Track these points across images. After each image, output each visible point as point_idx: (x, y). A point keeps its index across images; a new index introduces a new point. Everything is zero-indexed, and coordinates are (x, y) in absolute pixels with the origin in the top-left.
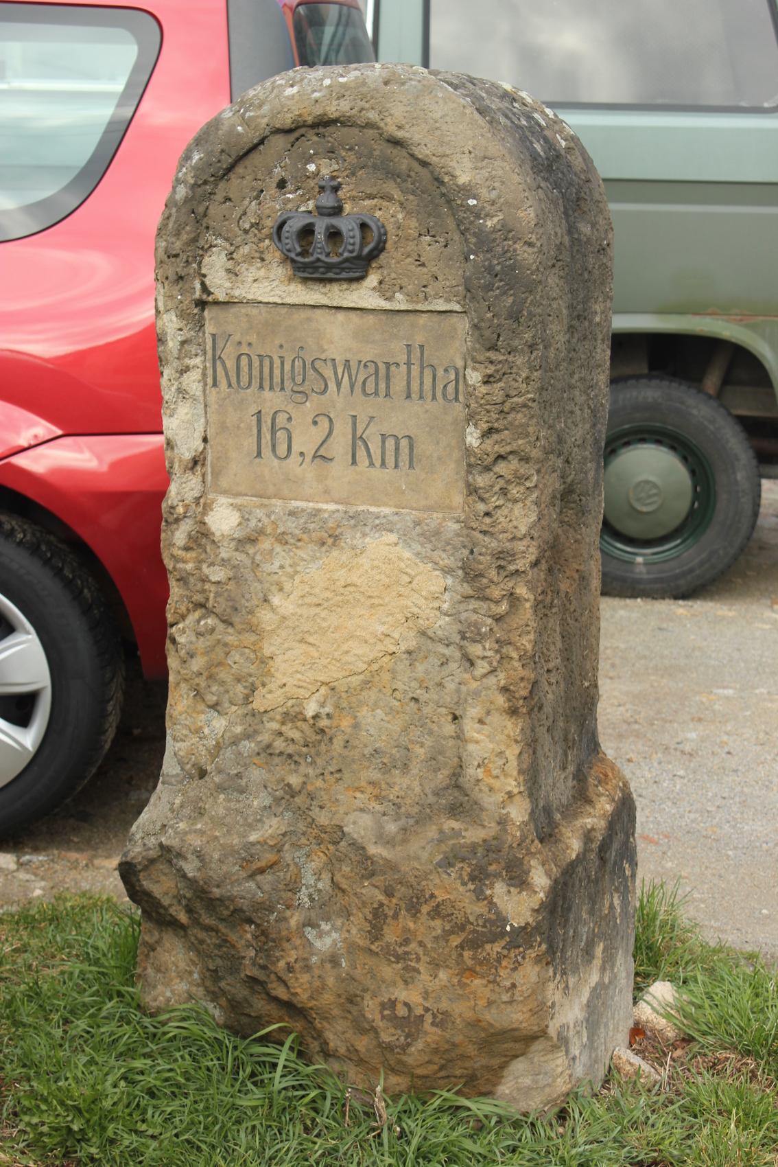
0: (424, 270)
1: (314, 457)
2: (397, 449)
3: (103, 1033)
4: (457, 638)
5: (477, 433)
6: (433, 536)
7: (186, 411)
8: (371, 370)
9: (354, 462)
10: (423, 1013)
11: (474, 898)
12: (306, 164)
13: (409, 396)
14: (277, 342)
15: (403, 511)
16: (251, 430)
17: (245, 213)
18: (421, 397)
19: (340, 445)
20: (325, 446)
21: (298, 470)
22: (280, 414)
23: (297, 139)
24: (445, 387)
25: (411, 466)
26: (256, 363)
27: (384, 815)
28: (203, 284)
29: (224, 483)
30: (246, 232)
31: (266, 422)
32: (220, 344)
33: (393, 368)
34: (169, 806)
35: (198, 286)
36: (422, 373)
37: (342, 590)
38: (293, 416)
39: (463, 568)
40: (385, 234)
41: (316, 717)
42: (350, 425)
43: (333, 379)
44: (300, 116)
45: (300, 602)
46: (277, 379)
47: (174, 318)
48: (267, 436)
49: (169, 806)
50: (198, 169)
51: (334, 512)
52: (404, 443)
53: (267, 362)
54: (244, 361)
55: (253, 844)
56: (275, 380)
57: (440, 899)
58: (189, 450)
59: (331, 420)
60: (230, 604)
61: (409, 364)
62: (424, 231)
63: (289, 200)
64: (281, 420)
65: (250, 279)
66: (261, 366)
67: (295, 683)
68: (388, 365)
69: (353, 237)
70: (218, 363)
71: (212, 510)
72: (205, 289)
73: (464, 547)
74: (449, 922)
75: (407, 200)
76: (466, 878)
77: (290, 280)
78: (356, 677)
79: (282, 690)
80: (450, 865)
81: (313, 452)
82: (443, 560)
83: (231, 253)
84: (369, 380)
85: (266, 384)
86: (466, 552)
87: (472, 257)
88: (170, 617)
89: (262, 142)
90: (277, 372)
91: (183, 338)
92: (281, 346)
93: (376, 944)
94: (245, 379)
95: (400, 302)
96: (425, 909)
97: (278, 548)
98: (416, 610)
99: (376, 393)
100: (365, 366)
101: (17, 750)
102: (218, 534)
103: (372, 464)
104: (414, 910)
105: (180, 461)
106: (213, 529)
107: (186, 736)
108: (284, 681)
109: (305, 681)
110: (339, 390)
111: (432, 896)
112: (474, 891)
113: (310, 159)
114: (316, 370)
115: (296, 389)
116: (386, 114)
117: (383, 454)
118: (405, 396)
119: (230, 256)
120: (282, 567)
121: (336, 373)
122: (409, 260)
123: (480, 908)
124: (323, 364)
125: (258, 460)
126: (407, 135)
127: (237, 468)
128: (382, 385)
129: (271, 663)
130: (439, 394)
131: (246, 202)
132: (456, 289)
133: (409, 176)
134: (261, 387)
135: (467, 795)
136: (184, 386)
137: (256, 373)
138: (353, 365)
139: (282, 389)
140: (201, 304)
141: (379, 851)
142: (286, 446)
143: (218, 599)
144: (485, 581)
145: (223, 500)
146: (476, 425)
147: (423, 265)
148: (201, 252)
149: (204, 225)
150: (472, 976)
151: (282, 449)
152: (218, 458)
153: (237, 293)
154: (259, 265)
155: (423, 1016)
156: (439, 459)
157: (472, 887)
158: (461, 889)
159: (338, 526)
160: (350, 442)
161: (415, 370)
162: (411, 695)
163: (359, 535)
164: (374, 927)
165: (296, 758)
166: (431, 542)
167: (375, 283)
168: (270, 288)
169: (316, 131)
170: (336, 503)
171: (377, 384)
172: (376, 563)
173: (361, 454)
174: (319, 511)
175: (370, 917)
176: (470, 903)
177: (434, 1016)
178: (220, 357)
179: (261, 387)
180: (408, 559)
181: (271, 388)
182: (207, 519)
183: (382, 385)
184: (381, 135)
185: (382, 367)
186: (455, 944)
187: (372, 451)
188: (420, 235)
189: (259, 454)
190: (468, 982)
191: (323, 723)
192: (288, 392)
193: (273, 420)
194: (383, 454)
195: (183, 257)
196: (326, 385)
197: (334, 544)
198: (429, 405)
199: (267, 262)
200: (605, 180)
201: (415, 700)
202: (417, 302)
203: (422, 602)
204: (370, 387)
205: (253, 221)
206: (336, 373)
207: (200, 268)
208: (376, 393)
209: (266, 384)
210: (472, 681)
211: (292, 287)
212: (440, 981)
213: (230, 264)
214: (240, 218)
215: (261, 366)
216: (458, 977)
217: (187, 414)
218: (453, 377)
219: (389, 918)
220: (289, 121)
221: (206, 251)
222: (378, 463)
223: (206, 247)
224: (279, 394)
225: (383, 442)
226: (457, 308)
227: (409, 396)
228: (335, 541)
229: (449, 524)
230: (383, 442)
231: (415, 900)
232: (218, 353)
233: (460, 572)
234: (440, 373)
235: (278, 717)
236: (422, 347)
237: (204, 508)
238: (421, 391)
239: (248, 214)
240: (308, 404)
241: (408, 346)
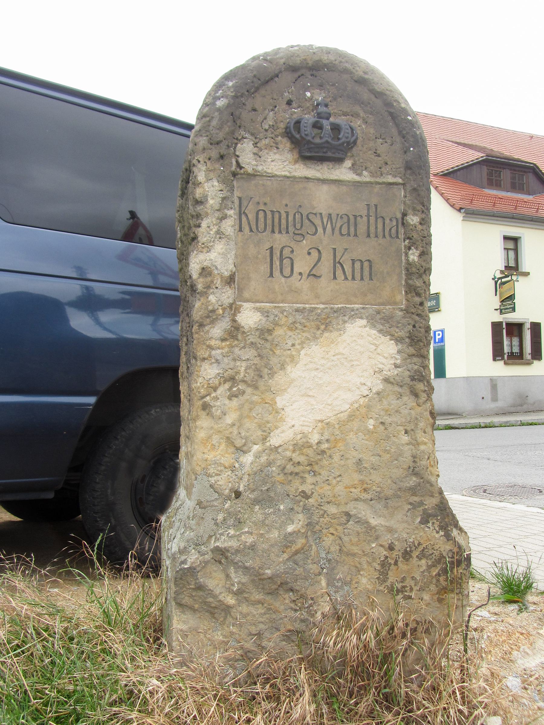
0: (380, 158)
2: (362, 268)
3: (168, 697)
4: (408, 380)
5: (417, 253)
6: (387, 319)
7: (221, 247)
8: (345, 219)
9: (335, 278)
10: (416, 626)
11: (445, 540)
12: (305, 91)
13: (369, 236)
14: (284, 202)
15: (367, 306)
16: (266, 259)
17: (265, 119)
18: (376, 236)
19: (325, 267)
20: (316, 268)
21: (298, 284)
22: (286, 248)
23: (299, 77)
24: (390, 230)
25: (371, 279)
26: (269, 216)
27: (371, 500)
28: (238, 163)
29: (246, 295)
30: (266, 130)
31: (276, 254)
32: (245, 203)
33: (359, 218)
34: (213, 522)
35: (234, 163)
36: (376, 221)
37: (333, 358)
38: (294, 249)
39: (409, 337)
41: (319, 443)
42: (332, 254)
43: (321, 226)
44: (305, 60)
45: (304, 369)
46: (284, 226)
47: (216, 183)
48: (277, 263)
49: (213, 522)
50: (237, 87)
51: (324, 309)
52: (366, 264)
53: (277, 216)
54: (261, 214)
55: (290, 534)
56: (282, 227)
57: (424, 545)
58: (227, 270)
59: (319, 251)
60: (257, 373)
61: (368, 216)
62: (378, 136)
63: (295, 113)
64: (287, 252)
65: (269, 160)
66: (273, 218)
67: (301, 423)
68: (355, 217)
70: (243, 217)
71: (239, 312)
73: (409, 324)
74: (431, 559)
75: (368, 117)
76: (437, 529)
77: (296, 162)
78: (343, 414)
79: (292, 429)
81: (308, 271)
82: (397, 333)
83: (256, 144)
84: (344, 226)
85: (276, 230)
86: (410, 327)
87: (412, 149)
89: (272, 79)
90: (284, 222)
91: (224, 196)
92: (286, 205)
93: (383, 586)
94: (261, 226)
95: (366, 177)
96: (415, 554)
97: (290, 333)
98: (381, 366)
99: (349, 235)
100: (341, 217)
101: (20, 521)
102: (246, 327)
103: (346, 278)
105: (222, 277)
106: (243, 324)
107: (221, 471)
108: (293, 423)
109: (307, 422)
110: (324, 232)
111: (419, 544)
112: (444, 536)
113: (307, 89)
115: (296, 232)
116: (356, 65)
117: (353, 271)
118: (366, 235)
119: (255, 145)
120: (293, 345)
122: (370, 152)
123: (448, 547)
124: (314, 216)
125: (270, 279)
126: (371, 78)
128: (352, 229)
129: (283, 412)
131: (267, 112)
132: (399, 169)
133: (369, 103)
134: (273, 231)
135: (422, 478)
136: (222, 229)
137: (269, 222)
138: (334, 217)
140: (234, 174)
141: (379, 522)
142: (289, 269)
143: (248, 371)
145: (246, 305)
146: (417, 248)
147: (379, 156)
148: (236, 141)
149: (238, 124)
150: (445, 593)
151: (287, 272)
152: (243, 279)
153: (260, 168)
154: (275, 151)
155: (416, 628)
156: (388, 273)
157: (443, 533)
158: (437, 536)
159: (328, 317)
160: (332, 265)
161: (372, 220)
162: (381, 420)
163: (341, 322)
164: (382, 573)
165: (302, 475)
166: (389, 322)
167: (350, 165)
168: (282, 166)
169: (311, 72)
170: (323, 304)
171: (349, 228)
172: (354, 338)
173: (339, 272)
174: (315, 308)
175: (378, 567)
176: (444, 544)
178: (244, 213)
179: (273, 231)
180: (374, 334)
181: (280, 232)
182: (237, 318)
183: (352, 229)
184: (352, 78)
186: (434, 573)
187: (346, 270)
188: (376, 138)
189: (271, 275)
190: (444, 597)
192: (291, 234)
193: (281, 252)
194: (353, 271)
195: (225, 143)
196: (316, 230)
197: (325, 329)
198: (381, 240)
199: (281, 149)
201: (382, 423)
202: (376, 177)
203: (384, 361)
205: (271, 124)
207: (235, 151)
208: (349, 235)
209: (276, 230)
210: (417, 407)
211: (297, 166)
212: (426, 601)
213: (255, 150)
214: (263, 121)
215: (273, 218)
216: (437, 596)
217: (222, 249)
218: (394, 223)
219: (392, 566)
220: (299, 62)
221: (240, 140)
222: (350, 278)
223: (240, 138)
224: (285, 235)
225: (353, 264)
226: (400, 181)
227: (369, 236)
228: (326, 326)
229: (397, 312)
230: (353, 264)
231: (408, 549)
232: (243, 209)
233: (407, 340)
234: (387, 221)
235: (291, 448)
236: (376, 206)
237: (235, 311)
238: (376, 232)
239: (268, 119)
240: (304, 241)
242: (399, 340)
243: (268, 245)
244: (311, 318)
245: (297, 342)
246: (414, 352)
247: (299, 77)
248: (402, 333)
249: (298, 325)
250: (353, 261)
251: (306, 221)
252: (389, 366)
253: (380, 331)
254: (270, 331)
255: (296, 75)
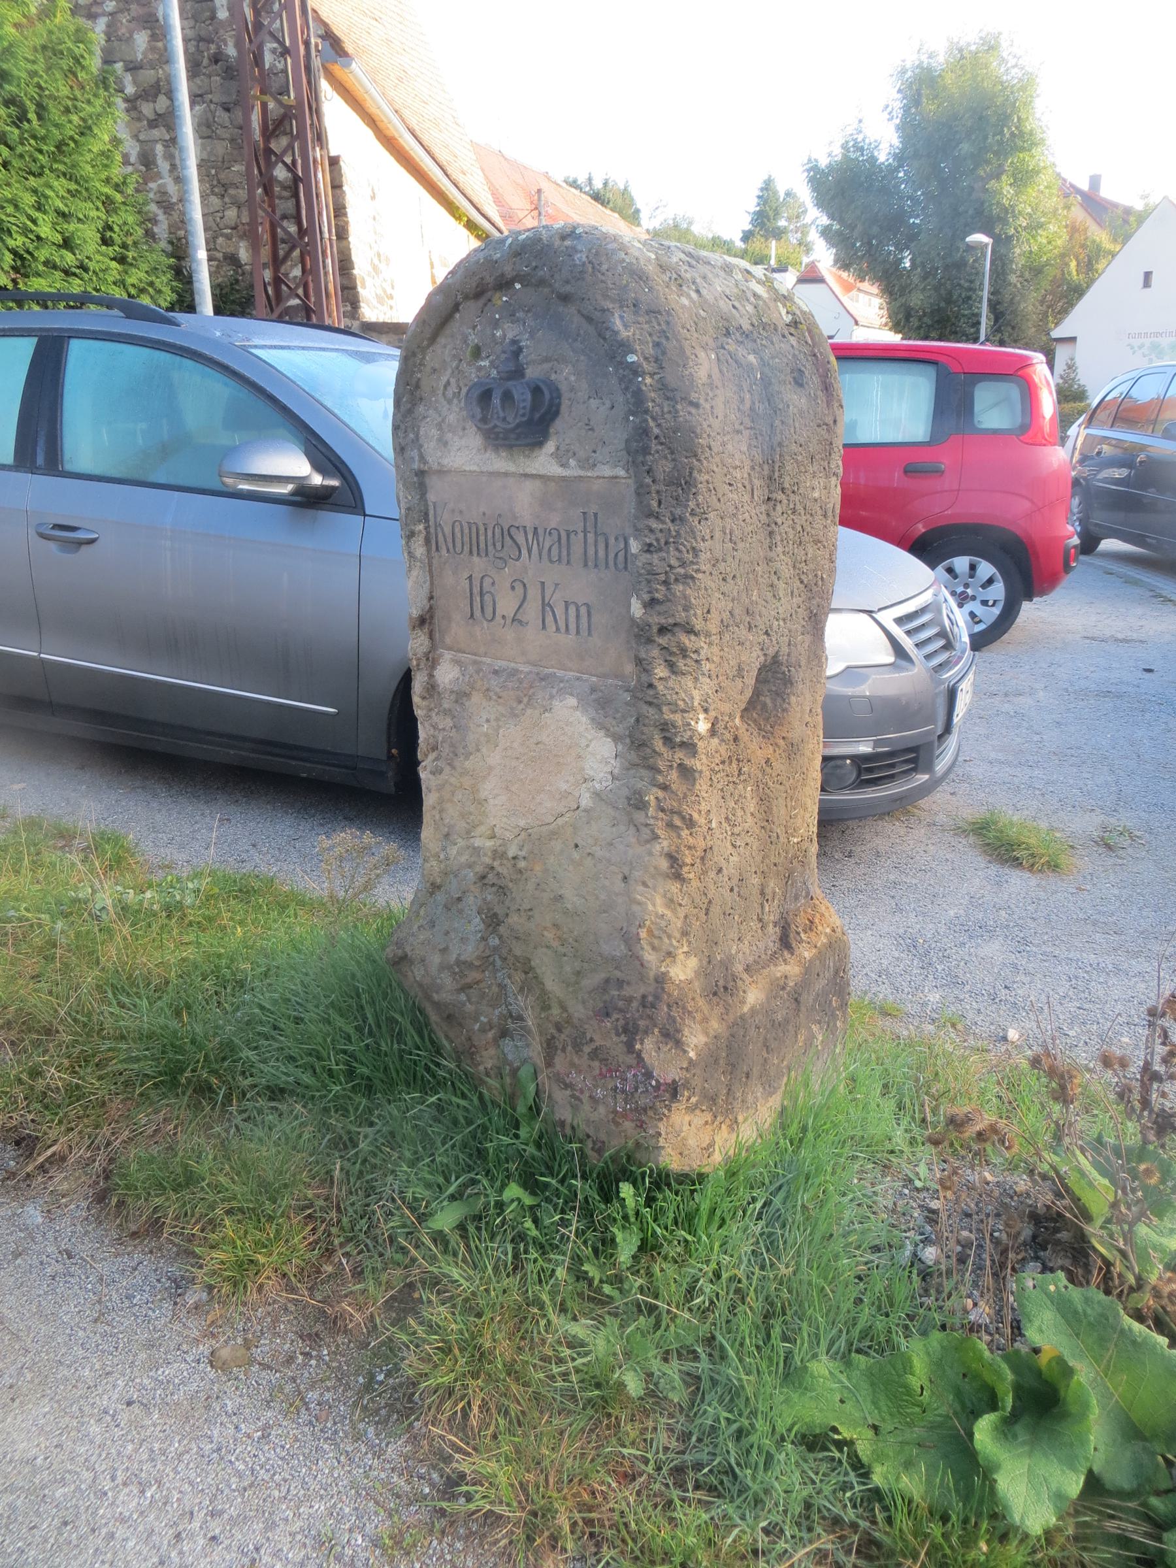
1: (513, 620)
2: (578, 616)
9: (544, 627)
13: (586, 565)
18: (596, 566)
19: (532, 611)
24: (616, 555)
25: (590, 634)
33: (572, 536)
39: (630, 736)
40: (559, 397)
46: (482, 546)
48: (477, 605)
52: (583, 610)
57: (597, 1044)
59: (525, 585)
61: (585, 532)
64: (487, 581)
69: (524, 401)
72: (422, 458)
80: (608, 1015)
85: (475, 552)
88: (420, 757)
90: (482, 538)
94: (458, 549)
95: (573, 470)
103: (558, 630)
104: (577, 1047)
111: (592, 1040)
114: (511, 537)
115: (497, 555)
121: (527, 540)
127: (456, 629)
128: (564, 553)
130: (611, 563)
134: (471, 552)
138: (540, 531)
139: (487, 555)
144: (648, 751)
145: (448, 655)
147: (592, 429)
157: (625, 1039)
159: (531, 687)
161: (591, 536)
171: (560, 552)
173: (549, 619)
177: (594, 1143)
179: (471, 552)
181: (478, 554)
185: (563, 534)
191: (522, 864)
194: (567, 620)
200: (836, 348)
204: (555, 552)
206: (527, 540)
208: (560, 560)
209: (475, 552)
218: (622, 546)
222: (563, 628)
224: (484, 559)
225: (567, 609)
230: (567, 609)
234: (612, 541)
241: (584, 513)
242: (616, 738)
243: (466, 575)
244: (510, 685)
245: (493, 717)
246: (637, 761)
247: (485, 305)
248: (620, 729)
249: (491, 694)
250: (567, 604)
251: (507, 538)
252: (602, 775)
253: (593, 719)
254: (467, 695)
255: (482, 301)
